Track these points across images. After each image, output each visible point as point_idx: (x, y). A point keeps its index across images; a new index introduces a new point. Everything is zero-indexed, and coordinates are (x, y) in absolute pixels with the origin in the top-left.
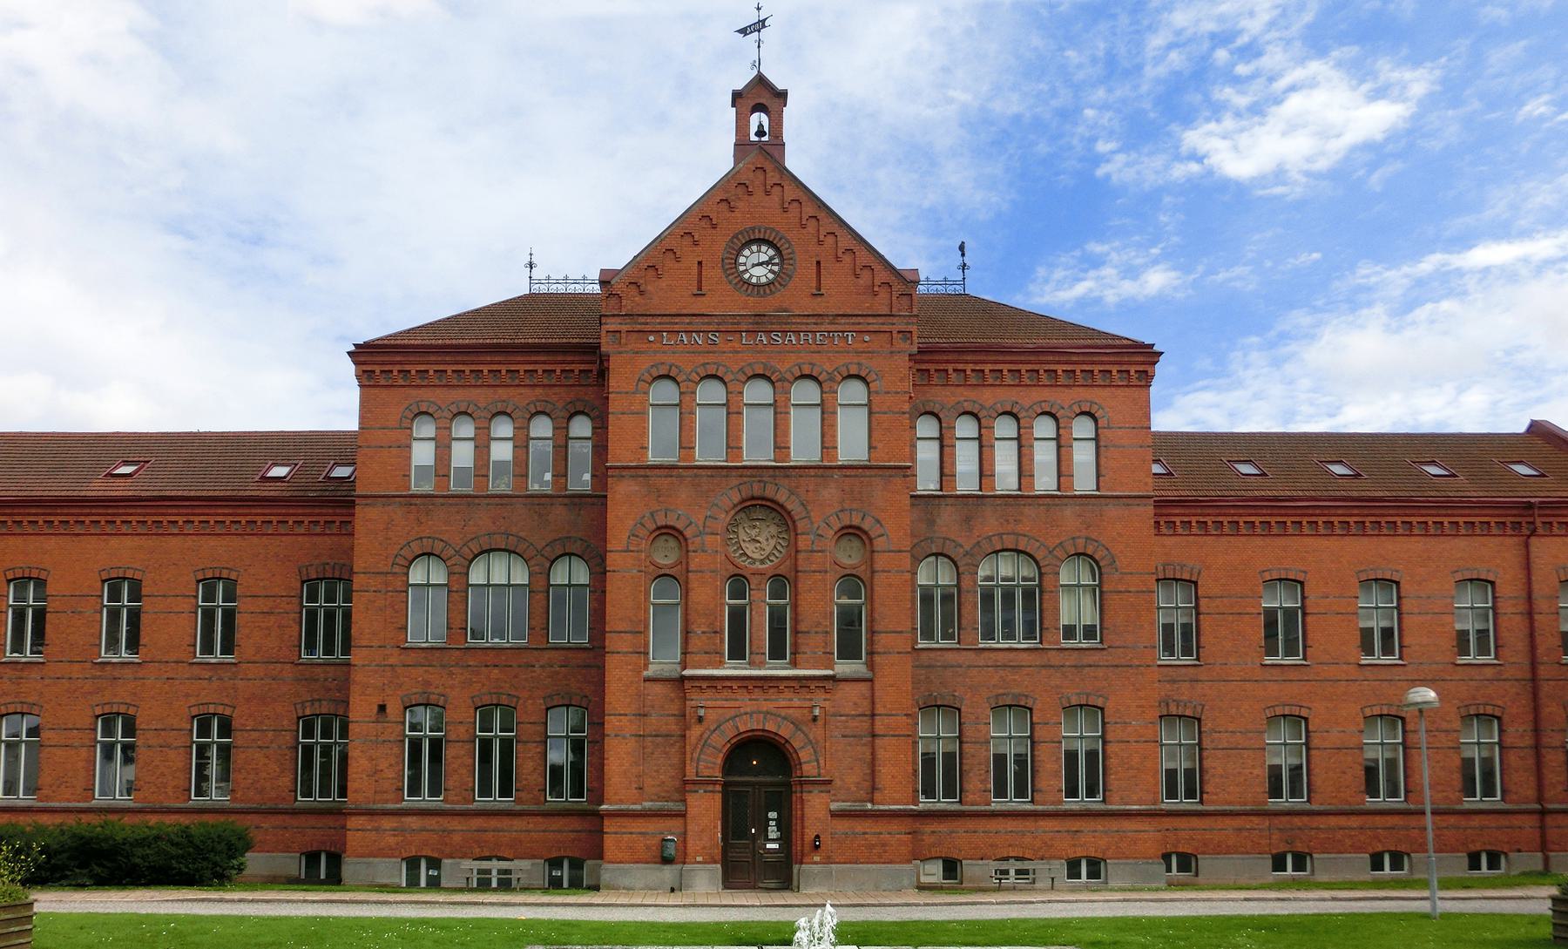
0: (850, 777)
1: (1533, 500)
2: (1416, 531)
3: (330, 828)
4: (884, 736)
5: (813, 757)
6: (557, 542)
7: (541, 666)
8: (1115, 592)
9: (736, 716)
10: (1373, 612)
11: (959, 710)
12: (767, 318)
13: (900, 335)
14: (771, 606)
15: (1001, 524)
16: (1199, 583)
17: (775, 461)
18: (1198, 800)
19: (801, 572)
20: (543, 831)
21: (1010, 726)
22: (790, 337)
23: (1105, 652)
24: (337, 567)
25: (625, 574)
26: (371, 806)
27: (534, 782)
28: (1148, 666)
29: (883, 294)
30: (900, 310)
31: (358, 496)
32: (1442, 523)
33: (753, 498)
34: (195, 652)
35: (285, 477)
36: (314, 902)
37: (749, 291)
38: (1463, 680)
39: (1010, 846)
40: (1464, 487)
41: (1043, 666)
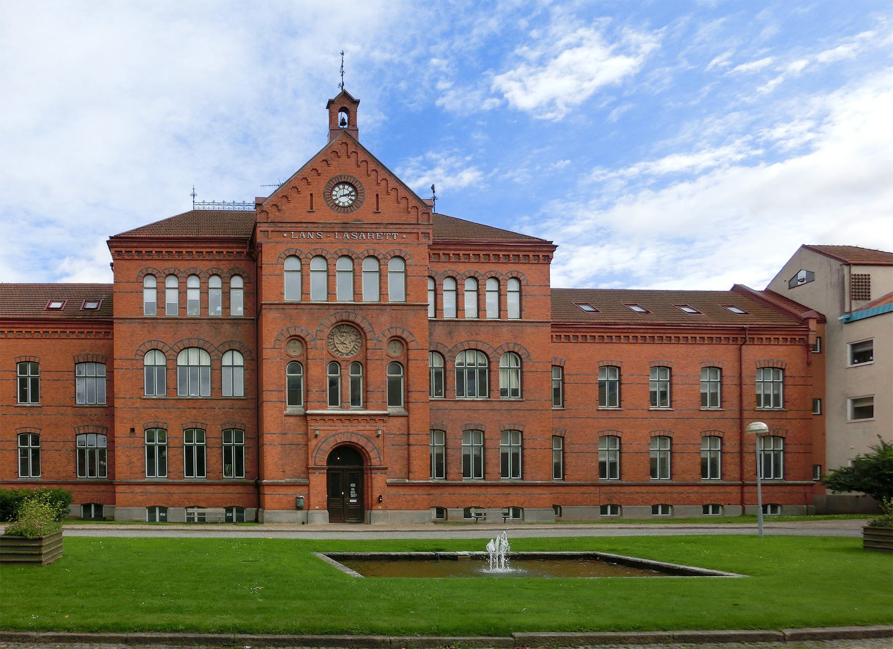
0: (396, 467)
1: (745, 326)
2: (681, 342)
3: (96, 492)
4: (415, 445)
5: (377, 456)
6: (226, 343)
7: (219, 408)
8: (530, 372)
9: (336, 435)
10: (656, 382)
11: (445, 432)
12: (349, 225)
13: (423, 235)
14: (351, 377)
15: (468, 335)
16: (565, 367)
17: (354, 301)
18: (444, 478)
19: (369, 359)
20: (223, 493)
21: (434, 439)
22: (346, 235)
23: (524, 403)
24: (94, 356)
25: (273, 360)
26: (129, 481)
27: (217, 468)
28: (547, 410)
29: (413, 212)
30: (423, 222)
31: (115, 319)
32: (695, 338)
33: (342, 321)
34: (17, 401)
35: (61, 308)
36: (122, 530)
37: (339, 210)
38: (704, 418)
39: (472, 501)
40: (704, 318)
41: (490, 410)
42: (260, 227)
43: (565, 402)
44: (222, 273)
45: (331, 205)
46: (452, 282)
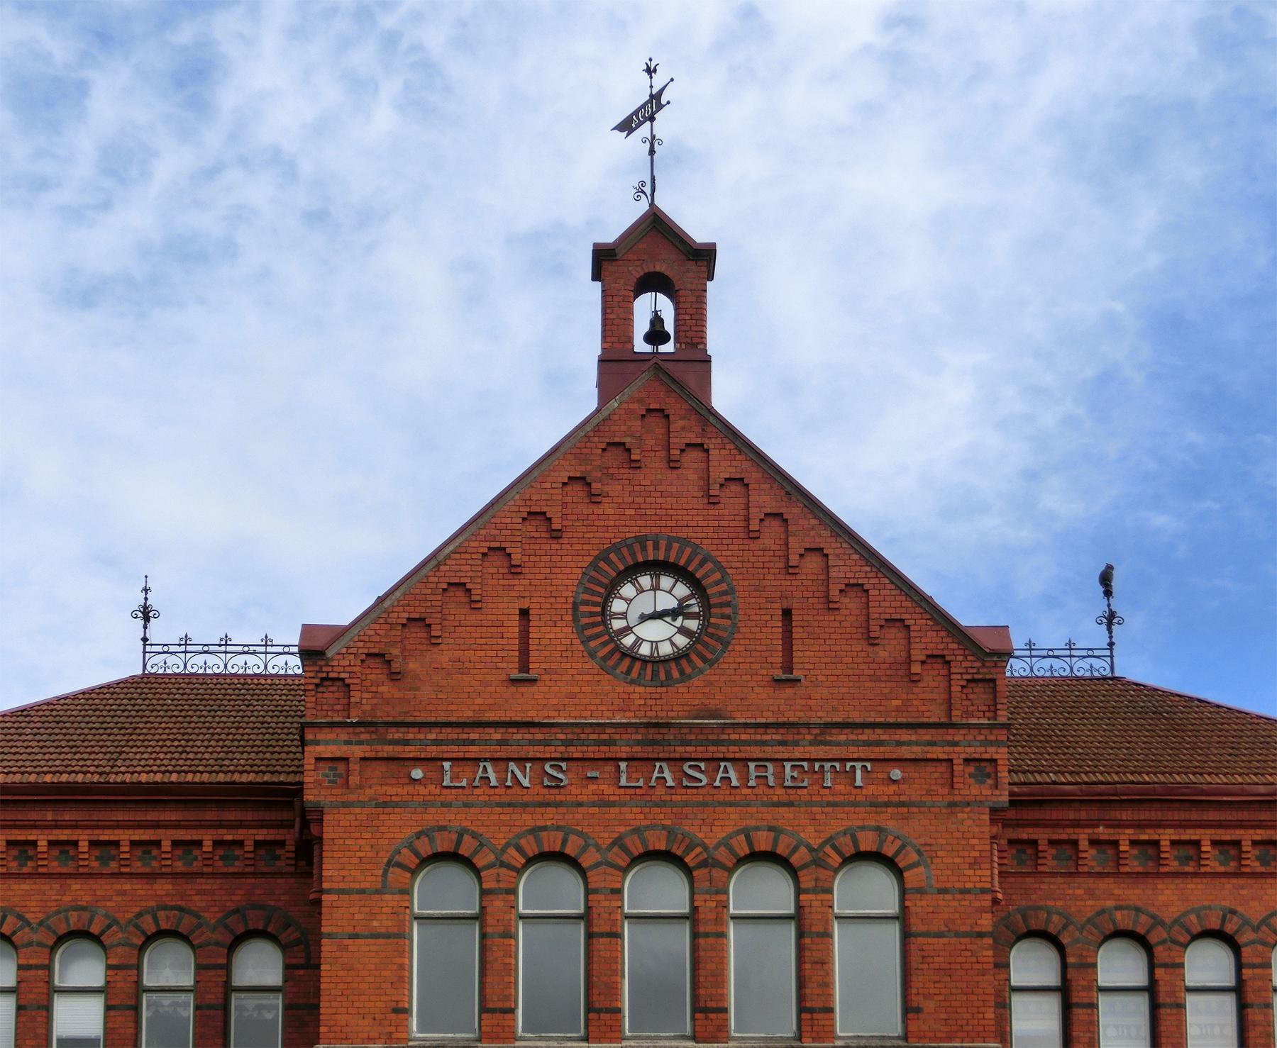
22: (726, 771)
29: (932, 680)
37: (634, 674)
42: (317, 743)
44: (200, 926)
45: (600, 654)
46: (1222, 951)
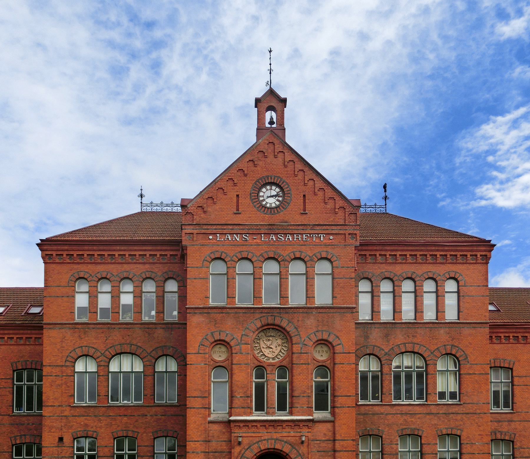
11: (382, 437)
13: (350, 236)
14: (278, 383)
17: (280, 304)
19: (295, 364)
23: (461, 406)
24: (34, 363)
28: (485, 413)
29: (341, 213)
31: (45, 324)
33: (268, 325)
37: (265, 212)
41: (427, 414)
42: (185, 229)
43: (514, 404)
45: (257, 206)
